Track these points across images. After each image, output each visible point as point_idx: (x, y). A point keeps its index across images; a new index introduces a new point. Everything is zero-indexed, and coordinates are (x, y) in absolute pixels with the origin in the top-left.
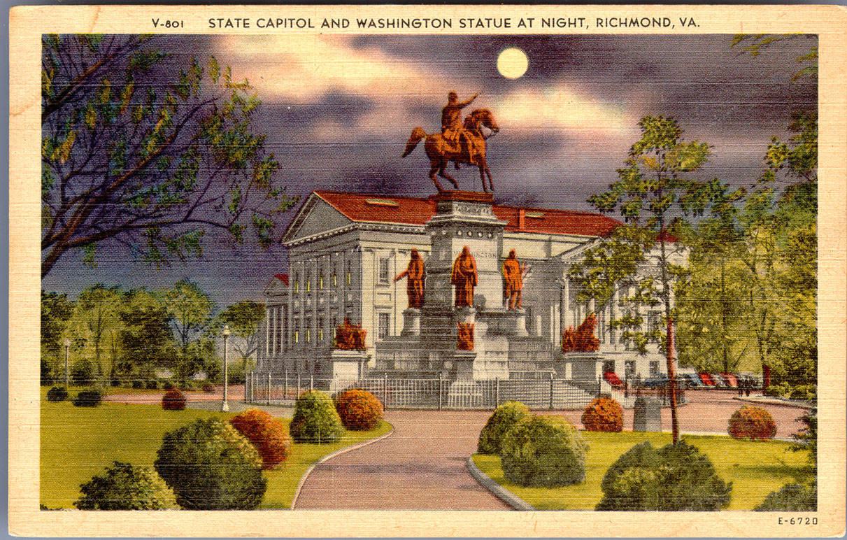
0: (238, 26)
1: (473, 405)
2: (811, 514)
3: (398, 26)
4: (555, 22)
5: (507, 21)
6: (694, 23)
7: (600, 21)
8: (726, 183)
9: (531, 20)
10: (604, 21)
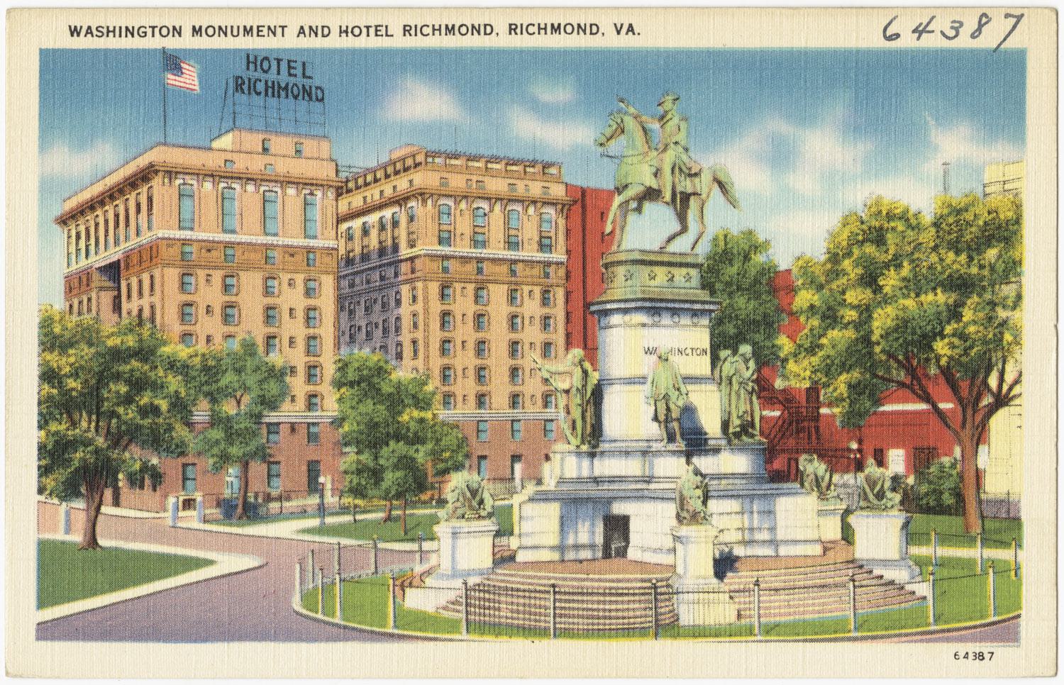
7: (513, 27)
8: (573, 278)
9: (283, 27)
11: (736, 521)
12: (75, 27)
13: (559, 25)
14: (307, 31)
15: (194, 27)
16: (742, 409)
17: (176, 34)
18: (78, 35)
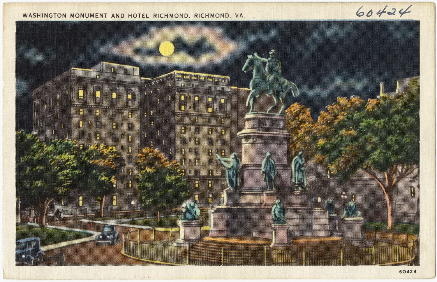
0: (55, 17)
1: (399, 261)
2: (414, 268)
3: (42, 17)
4: (159, 16)
5: (97, 15)
6: (242, 16)
9: (106, 14)
10: (198, 15)
11: (296, 222)
12: (25, 14)
13: (173, 14)
14: (115, 16)
15: (71, 14)
16: (300, 177)
17: (64, 16)
18: (26, 17)
